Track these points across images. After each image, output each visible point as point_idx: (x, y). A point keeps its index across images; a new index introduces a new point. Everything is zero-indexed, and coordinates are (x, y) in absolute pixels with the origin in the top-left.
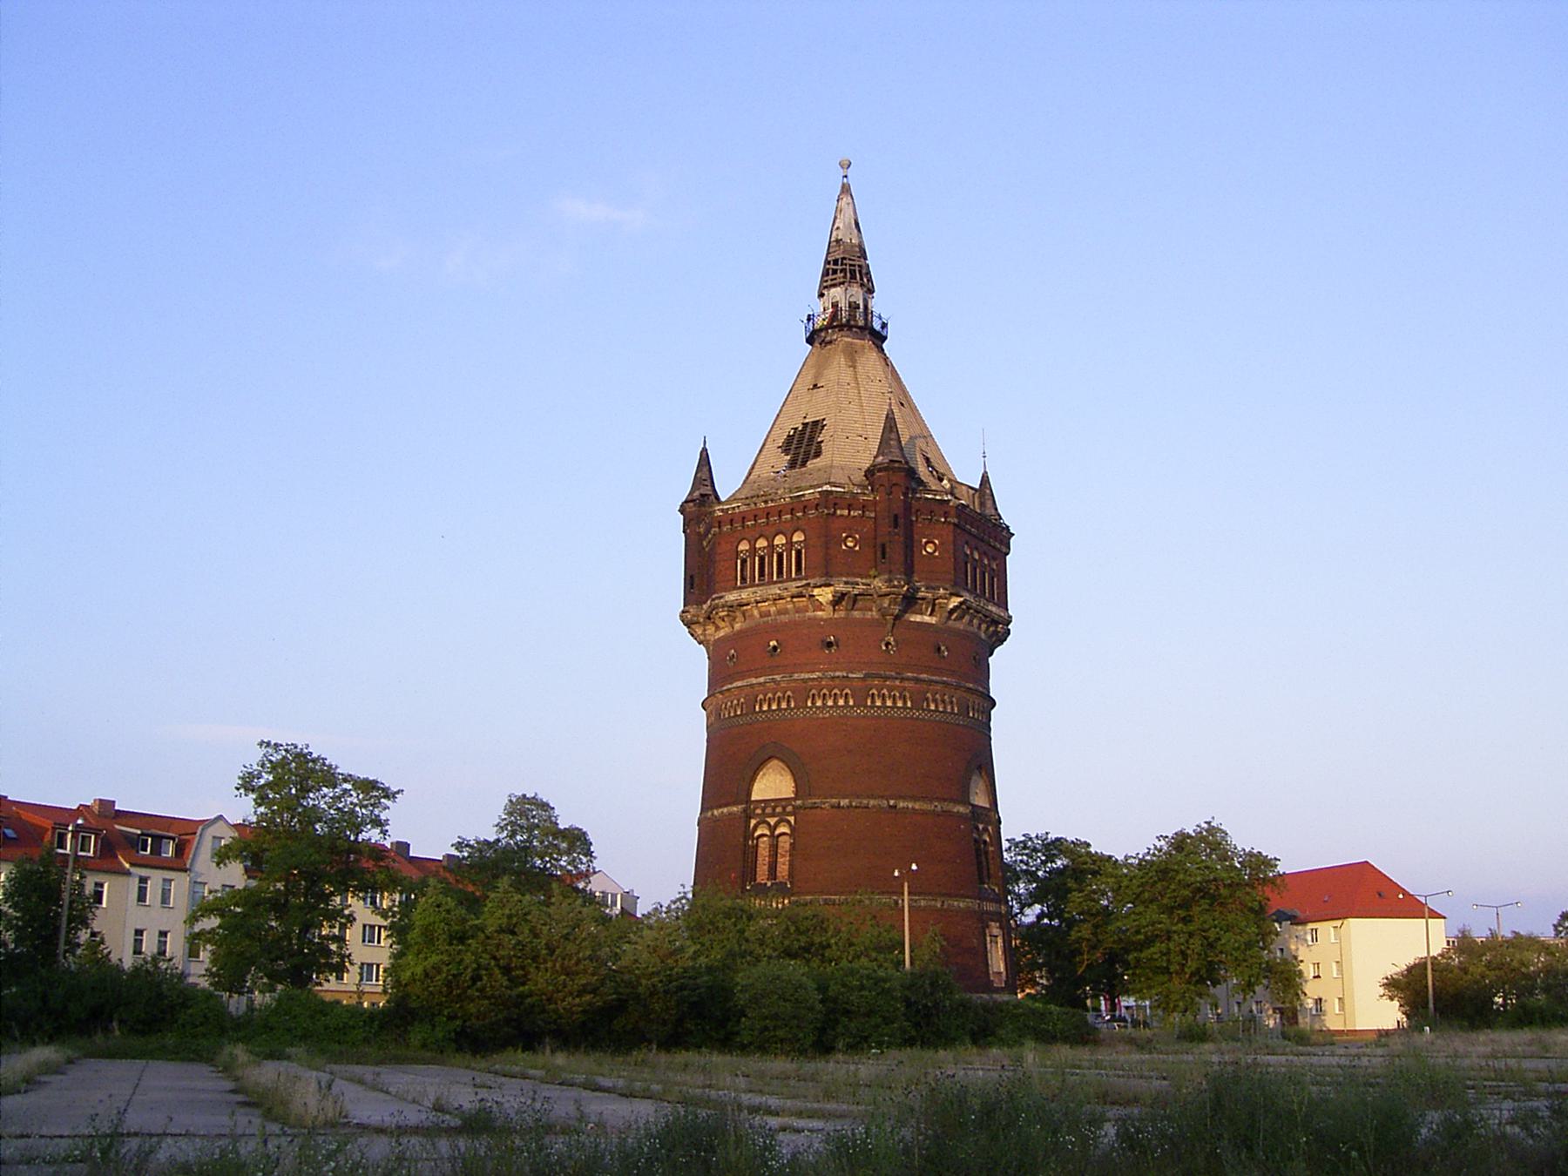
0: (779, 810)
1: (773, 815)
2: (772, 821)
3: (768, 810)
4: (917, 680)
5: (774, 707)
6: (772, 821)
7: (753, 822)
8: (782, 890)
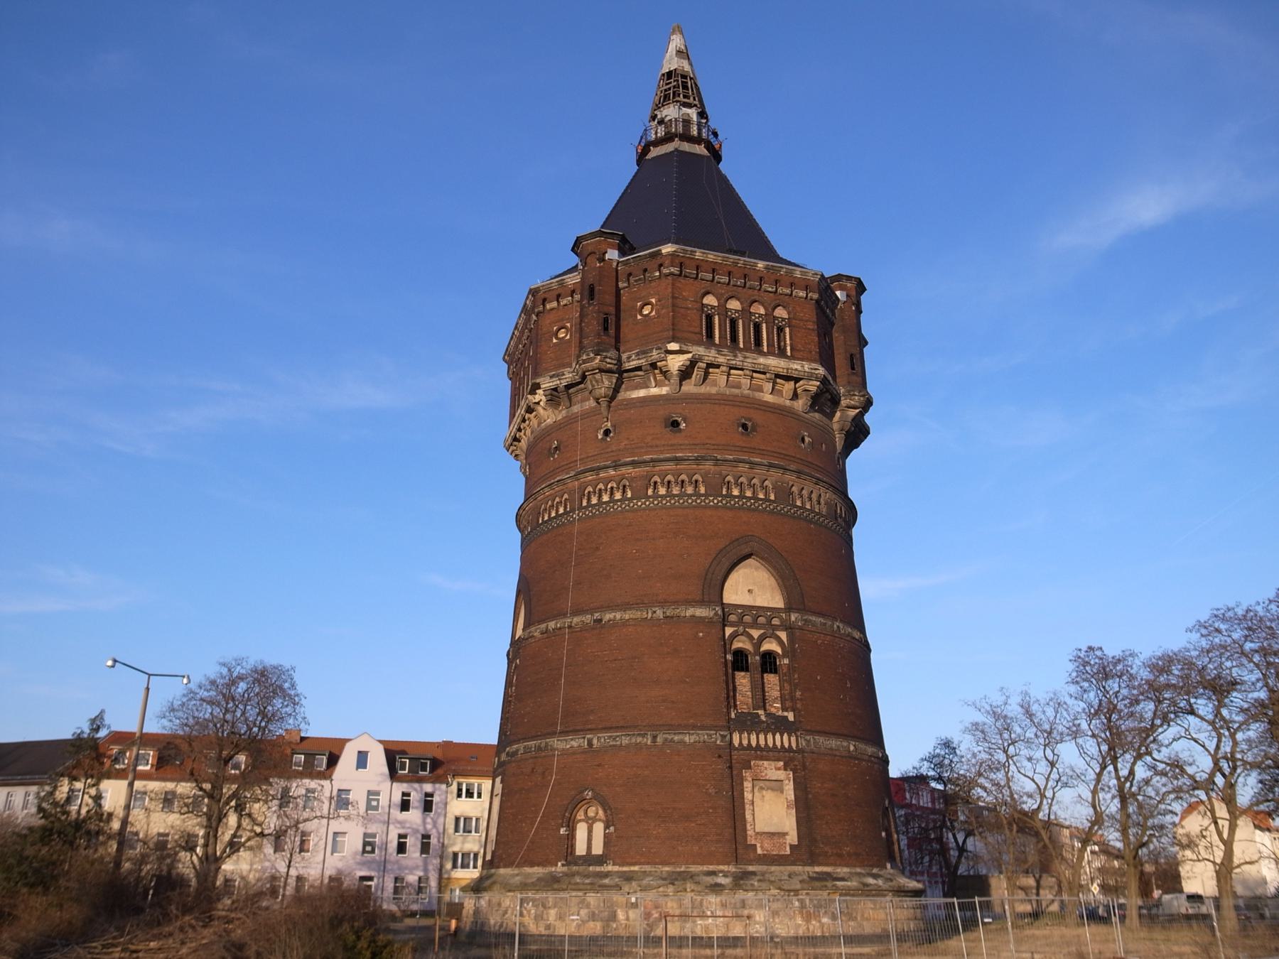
0: (762, 620)
1: (755, 625)
2: (756, 634)
3: (747, 619)
5: (606, 498)
6: (756, 634)
7: (729, 631)
8: (779, 725)
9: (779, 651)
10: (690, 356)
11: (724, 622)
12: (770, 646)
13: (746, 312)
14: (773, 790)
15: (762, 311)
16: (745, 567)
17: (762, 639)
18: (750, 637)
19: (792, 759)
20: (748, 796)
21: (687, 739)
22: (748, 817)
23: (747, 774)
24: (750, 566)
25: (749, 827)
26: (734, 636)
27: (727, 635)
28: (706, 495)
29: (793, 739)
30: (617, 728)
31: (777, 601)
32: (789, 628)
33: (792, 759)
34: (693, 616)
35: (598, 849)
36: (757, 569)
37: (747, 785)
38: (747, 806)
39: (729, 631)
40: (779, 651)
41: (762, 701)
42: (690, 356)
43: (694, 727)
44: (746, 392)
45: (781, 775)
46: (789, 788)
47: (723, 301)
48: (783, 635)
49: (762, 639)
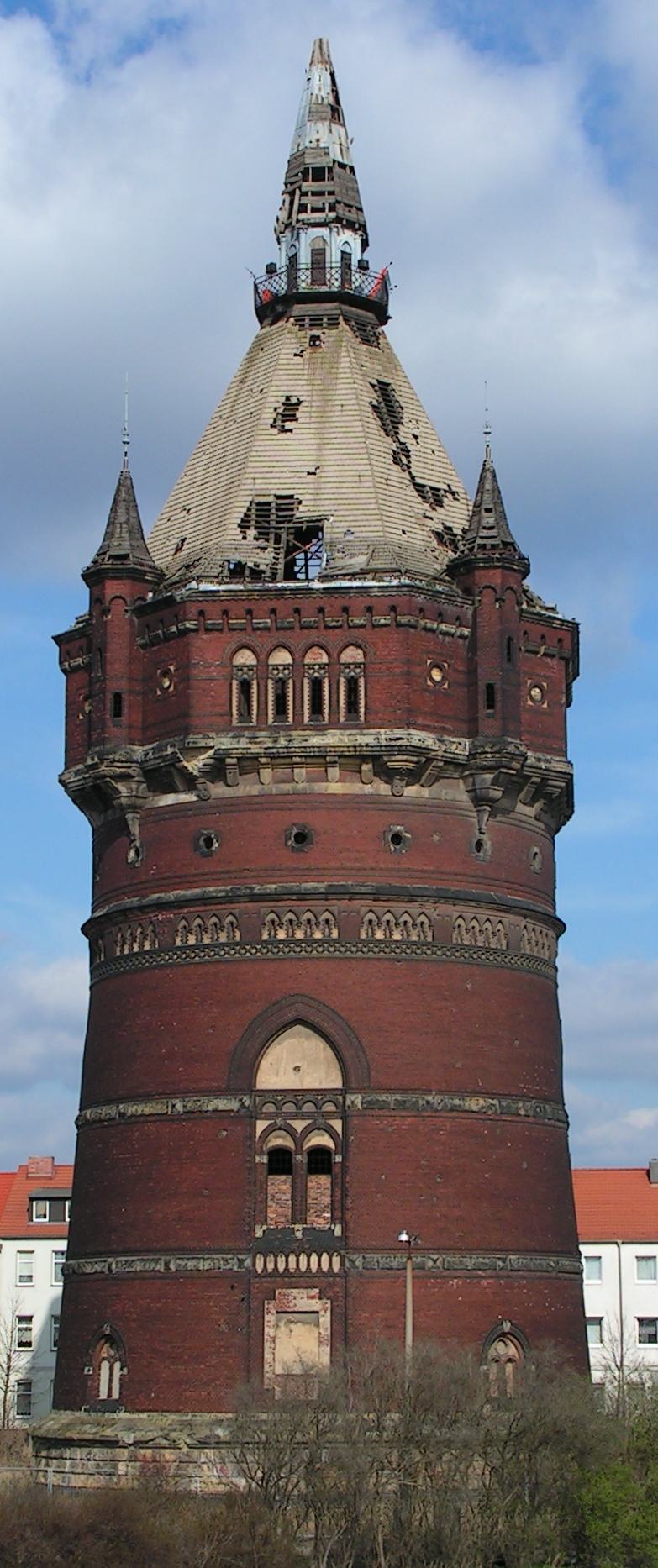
4: (204, 900)
6: (299, 1125)
7: (261, 1125)
8: (318, 1243)
9: (332, 1145)
10: (211, 752)
11: (254, 1116)
12: (324, 1140)
13: (297, 667)
14: (303, 1323)
15: (325, 659)
16: (292, 1036)
17: (307, 1131)
18: (291, 1132)
19: (331, 1285)
20: (269, 1331)
21: (467, 1261)
22: (268, 1356)
23: (270, 1306)
24: (299, 1034)
25: (267, 1367)
26: (267, 1132)
27: (332, 1122)
28: (242, 944)
29: (336, 1260)
30: (133, 1252)
31: (332, 1079)
32: (344, 1114)
33: (331, 1285)
34: (215, 1111)
35: (116, 1395)
36: (308, 1037)
37: (270, 1318)
38: (267, 1345)
39: (261, 1125)
40: (332, 1145)
41: (299, 1209)
42: (211, 752)
43: (210, 1251)
44: (300, 786)
45: (315, 1305)
46: (325, 1319)
47: (262, 656)
48: (337, 1125)
49: (307, 1131)
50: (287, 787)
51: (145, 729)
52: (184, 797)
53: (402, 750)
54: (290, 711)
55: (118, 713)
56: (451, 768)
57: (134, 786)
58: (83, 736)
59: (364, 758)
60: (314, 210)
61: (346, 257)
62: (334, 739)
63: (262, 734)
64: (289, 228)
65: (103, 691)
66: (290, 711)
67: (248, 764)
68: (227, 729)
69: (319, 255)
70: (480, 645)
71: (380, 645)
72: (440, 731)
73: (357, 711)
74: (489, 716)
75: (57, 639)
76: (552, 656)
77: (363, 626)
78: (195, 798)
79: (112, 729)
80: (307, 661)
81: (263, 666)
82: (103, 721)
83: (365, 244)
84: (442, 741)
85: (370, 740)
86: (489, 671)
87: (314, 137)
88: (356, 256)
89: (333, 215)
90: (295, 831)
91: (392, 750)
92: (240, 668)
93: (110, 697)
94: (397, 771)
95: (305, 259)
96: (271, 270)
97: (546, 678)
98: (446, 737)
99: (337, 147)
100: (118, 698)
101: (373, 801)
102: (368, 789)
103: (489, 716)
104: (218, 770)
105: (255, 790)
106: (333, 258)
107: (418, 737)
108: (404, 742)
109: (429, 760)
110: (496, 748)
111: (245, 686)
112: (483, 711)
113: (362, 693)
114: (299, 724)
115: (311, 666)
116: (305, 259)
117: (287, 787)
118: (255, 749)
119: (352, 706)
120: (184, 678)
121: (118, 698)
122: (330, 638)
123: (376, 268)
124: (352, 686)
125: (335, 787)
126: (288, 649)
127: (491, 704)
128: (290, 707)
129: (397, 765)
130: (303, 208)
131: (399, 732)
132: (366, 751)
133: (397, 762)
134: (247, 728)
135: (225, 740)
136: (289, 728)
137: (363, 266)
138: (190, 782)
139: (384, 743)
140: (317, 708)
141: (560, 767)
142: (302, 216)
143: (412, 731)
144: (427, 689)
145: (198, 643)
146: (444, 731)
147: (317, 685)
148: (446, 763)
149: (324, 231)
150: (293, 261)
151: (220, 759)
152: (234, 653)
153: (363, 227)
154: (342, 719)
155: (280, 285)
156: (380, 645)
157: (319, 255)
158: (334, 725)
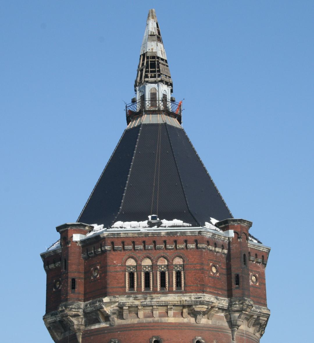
10: (117, 304)
15: (166, 263)
42: (117, 304)
50: (150, 320)
51: (85, 294)
52: (103, 325)
53: (202, 303)
54: (151, 286)
55: (73, 287)
56: (221, 311)
57: (80, 320)
58: (55, 299)
59: (184, 306)
60: (151, 77)
61: (165, 96)
62: (172, 298)
63: (140, 296)
64: (139, 84)
65: (67, 278)
66: (151, 286)
67: (134, 310)
68: (124, 293)
69: (154, 96)
70: (232, 257)
71: (191, 257)
72: (216, 295)
73: (181, 286)
74: (237, 288)
75: (43, 256)
76: (259, 263)
77: (183, 249)
78: (108, 326)
79: (71, 295)
80: (159, 263)
81: (138, 267)
82: (67, 291)
83: (172, 91)
84: (217, 299)
85: (187, 298)
86: (235, 269)
87: (150, 48)
88: (169, 97)
89: (159, 79)
90: (154, 339)
91: (197, 303)
92: (129, 267)
93: (70, 281)
94: (199, 313)
95: (148, 97)
96: (134, 101)
97: (258, 272)
98: (219, 297)
99: (160, 52)
100: (74, 281)
101: (188, 326)
102: (186, 320)
103: (237, 288)
104: (120, 313)
105: (136, 321)
106: (160, 96)
107: (208, 297)
108: (202, 299)
109: (212, 307)
110: (241, 302)
111: (131, 275)
112: (234, 286)
113: (183, 278)
114: (155, 291)
115: (160, 266)
116: (148, 97)
117: (150, 320)
118: (137, 303)
119: (179, 284)
120: (104, 271)
121: (74, 281)
122: (168, 254)
123: (177, 101)
124: (178, 274)
125: (171, 319)
126: (150, 258)
127: (237, 283)
128: (151, 284)
129: (198, 310)
130: (146, 76)
131: (199, 295)
132: (186, 303)
133: (198, 308)
134: (132, 293)
135: (122, 298)
136: (150, 293)
137: (172, 100)
138: (107, 318)
139: (193, 299)
140: (163, 285)
141: (265, 311)
142: (146, 79)
143: (205, 294)
144: (210, 276)
145: (111, 256)
146: (218, 294)
147: (163, 274)
148: (219, 309)
149: (155, 86)
150: (143, 98)
151: (121, 307)
152: (126, 260)
153: (171, 85)
154: (174, 289)
155: (137, 108)
156: (191, 257)
157: (154, 96)
158: (171, 291)
